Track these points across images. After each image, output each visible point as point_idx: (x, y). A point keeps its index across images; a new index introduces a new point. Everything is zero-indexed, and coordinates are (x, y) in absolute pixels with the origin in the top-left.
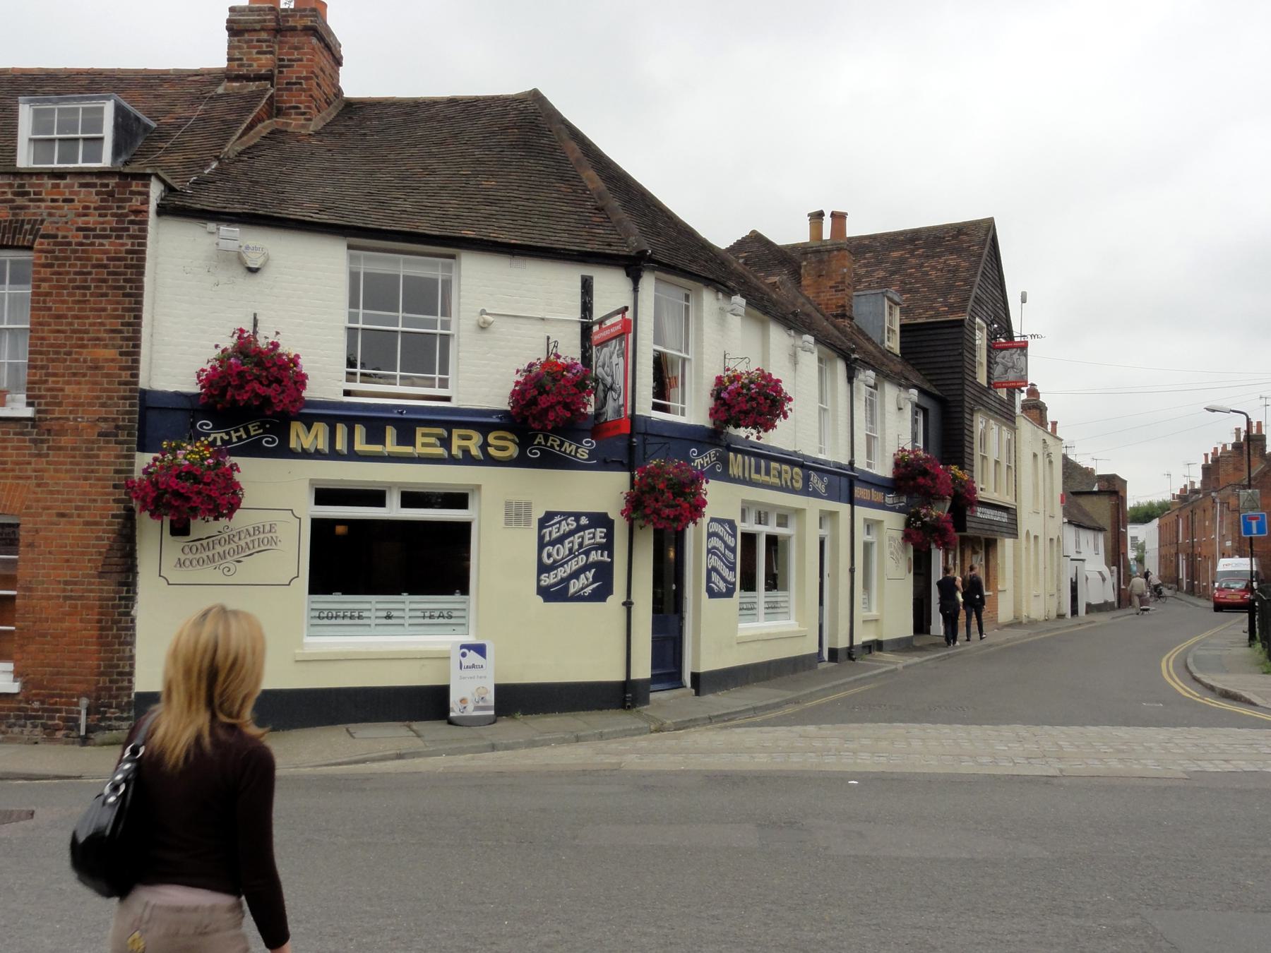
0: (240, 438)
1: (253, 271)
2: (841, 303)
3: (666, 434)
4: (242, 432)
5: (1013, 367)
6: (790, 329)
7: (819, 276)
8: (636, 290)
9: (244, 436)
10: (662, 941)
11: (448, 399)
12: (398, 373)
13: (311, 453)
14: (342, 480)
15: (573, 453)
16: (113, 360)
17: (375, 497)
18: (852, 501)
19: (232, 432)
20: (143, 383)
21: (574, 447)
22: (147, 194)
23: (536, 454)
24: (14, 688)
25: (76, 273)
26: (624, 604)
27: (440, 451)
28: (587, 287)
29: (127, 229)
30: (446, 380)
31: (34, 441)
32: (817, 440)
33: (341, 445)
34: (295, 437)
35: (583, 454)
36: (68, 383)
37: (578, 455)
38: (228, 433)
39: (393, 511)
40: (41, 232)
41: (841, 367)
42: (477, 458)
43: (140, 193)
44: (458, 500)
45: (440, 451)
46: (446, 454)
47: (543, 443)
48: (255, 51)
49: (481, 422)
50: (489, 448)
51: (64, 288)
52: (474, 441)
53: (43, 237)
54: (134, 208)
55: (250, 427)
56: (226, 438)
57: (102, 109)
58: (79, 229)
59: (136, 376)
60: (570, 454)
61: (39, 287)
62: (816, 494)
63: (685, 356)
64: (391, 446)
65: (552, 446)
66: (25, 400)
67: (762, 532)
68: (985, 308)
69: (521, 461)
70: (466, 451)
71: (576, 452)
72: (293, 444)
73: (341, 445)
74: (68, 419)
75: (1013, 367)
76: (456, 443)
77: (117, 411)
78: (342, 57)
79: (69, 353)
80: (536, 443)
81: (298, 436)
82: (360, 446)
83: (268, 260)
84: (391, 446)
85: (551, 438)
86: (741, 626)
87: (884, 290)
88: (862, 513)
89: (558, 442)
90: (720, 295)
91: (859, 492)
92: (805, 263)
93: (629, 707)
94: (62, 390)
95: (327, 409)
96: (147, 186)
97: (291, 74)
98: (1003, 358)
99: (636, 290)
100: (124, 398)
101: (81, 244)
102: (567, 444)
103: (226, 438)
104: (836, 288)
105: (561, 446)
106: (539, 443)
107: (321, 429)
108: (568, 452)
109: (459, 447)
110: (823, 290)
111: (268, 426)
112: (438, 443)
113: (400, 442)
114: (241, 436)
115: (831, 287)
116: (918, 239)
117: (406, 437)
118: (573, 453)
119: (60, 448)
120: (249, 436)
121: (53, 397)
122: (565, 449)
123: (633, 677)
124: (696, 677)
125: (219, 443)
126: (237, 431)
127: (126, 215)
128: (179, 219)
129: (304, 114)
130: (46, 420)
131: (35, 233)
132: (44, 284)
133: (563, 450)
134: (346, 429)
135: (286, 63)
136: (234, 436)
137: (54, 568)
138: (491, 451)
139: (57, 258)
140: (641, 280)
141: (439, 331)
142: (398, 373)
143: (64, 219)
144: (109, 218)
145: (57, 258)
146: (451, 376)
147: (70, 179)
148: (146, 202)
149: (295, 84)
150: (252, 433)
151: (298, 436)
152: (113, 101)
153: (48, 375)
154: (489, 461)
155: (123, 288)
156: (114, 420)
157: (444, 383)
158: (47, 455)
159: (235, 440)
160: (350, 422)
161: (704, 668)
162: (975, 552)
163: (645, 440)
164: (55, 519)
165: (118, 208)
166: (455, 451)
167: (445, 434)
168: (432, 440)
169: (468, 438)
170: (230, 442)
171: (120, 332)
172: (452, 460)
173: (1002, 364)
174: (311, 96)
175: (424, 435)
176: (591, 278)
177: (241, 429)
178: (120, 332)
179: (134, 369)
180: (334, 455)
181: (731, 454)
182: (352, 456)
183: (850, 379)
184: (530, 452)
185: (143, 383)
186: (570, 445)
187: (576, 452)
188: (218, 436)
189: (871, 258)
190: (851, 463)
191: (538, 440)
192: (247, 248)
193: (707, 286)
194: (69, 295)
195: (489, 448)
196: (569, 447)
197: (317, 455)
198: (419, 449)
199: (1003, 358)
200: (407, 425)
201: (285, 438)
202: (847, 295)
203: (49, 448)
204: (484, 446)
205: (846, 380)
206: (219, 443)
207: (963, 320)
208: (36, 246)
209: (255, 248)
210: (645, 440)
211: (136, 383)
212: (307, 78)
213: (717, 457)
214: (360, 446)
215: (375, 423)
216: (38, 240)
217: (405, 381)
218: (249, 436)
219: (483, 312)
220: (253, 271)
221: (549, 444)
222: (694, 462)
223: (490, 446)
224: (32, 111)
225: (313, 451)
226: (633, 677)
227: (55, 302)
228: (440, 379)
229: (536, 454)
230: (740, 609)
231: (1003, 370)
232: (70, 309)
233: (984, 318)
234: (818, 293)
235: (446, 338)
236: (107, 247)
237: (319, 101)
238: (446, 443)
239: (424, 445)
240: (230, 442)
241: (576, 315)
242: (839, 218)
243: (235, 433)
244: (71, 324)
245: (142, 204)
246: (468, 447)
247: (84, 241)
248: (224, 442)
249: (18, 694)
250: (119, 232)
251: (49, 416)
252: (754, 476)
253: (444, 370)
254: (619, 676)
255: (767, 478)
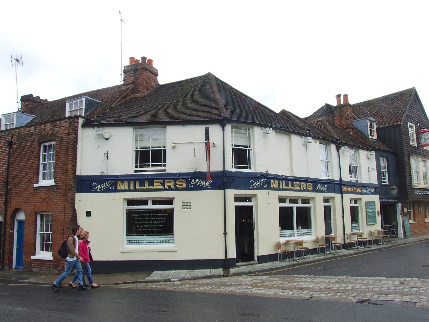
0: (104, 187)
1: (107, 139)
2: (348, 124)
3: (238, 176)
4: (104, 186)
5: (428, 139)
6: (302, 136)
7: (340, 116)
8: (223, 130)
9: (105, 187)
10: (388, 315)
11: (165, 171)
12: (150, 164)
13: (123, 190)
14: (132, 198)
15: (204, 185)
16: (71, 168)
17: (145, 202)
18: (341, 192)
19: (102, 186)
20: (78, 173)
21: (204, 183)
22: (78, 122)
23: (192, 186)
24: (51, 259)
25: (64, 146)
26: (224, 233)
27: (161, 187)
28: (207, 132)
29: (74, 132)
30: (165, 165)
31: (55, 192)
32: (236, 144)
33: (132, 187)
34: (119, 186)
35: (208, 185)
36: (62, 175)
37: (206, 185)
38: (101, 186)
39: (150, 206)
40: (57, 136)
41: (333, 147)
42: (173, 189)
43: (77, 122)
44: (170, 201)
45: (161, 187)
46: (163, 188)
47: (194, 182)
48: (129, 77)
49: (176, 177)
50: (177, 185)
51: (61, 150)
52: (172, 183)
53: (58, 137)
54: (76, 126)
55: (106, 184)
56: (100, 187)
57: (83, 100)
58: (65, 134)
59: (76, 172)
60: (203, 185)
61: (56, 150)
62: (321, 191)
63: (249, 149)
64: (146, 187)
65: (197, 183)
66: (54, 181)
67: (294, 206)
68: (413, 119)
69: (188, 189)
70: (169, 186)
71: (205, 184)
72: (118, 188)
73: (132, 187)
74: (62, 185)
75: (428, 139)
76: (166, 184)
77: (72, 182)
78: (158, 74)
79: (62, 167)
80: (192, 182)
81: (120, 185)
82: (137, 187)
83: (111, 135)
84: (146, 187)
85: (197, 180)
86: (280, 239)
87: (367, 117)
88: (347, 197)
89: (199, 182)
90: (263, 128)
91: (344, 189)
92: (335, 112)
93: (226, 268)
94: (61, 177)
95: (125, 177)
96: (78, 120)
97: (139, 81)
98: (424, 136)
99: (223, 130)
100: (73, 178)
101: (65, 138)
102: (202, 182)
103: (100, 187)
104: (346, 119)
105: (200, 183)
106: (193, 182)
107: (126, 183)
108: (202, 184)
109: (167, 185)
110: (342, 120)
111: (111, 183)
112: (161, 185)
113: (292, 186)
114: (104, 187)
115: (344, 119)
116: (388, 98)
117: (151, 184)
118: (204, 185)
119: (61, 193)
120: (106, 187)
121: (59, 179)
122: (202, 184)
123: (228, 258)
124: (258, 257)
125: (98, 189)
126: (103, 185)
127: (74, 128)
128: (199, 125)
129: (142, 91)
130: (58, 186)
131: (56, 136)
132: (58, 150)
133: (201, 184)
134: (133, 182)
135: (138, 78)
136: (102, 187)
137: (59, 226)
138: (177, 186)
139: (60, 142)
140: (225, 127)
141: (248, 148)
142: (150, 164)
143: (62, 132)
144: (70, 130)
145: (60, 142)
146: (167, 163)
147: (63, 121)
148: (78, 124)
149: (140, 84)
150: (107, 186)
151: (120, 185)
152: (85, 98)
153: (58, 174)
154: (177, 189)
155: (73, 148)
156: (71, 184)
157: (164, 166)
158: (58, 195)
159: (102, 188)
160: (134, 181)
161: (260, 254)
162: (419, 207)
163: (229, 179)
164: (60, 213)
165: (72, 127)
166: (166, 187)
167: (163, 182)
168: (159, 184)
169: (170, 182)
170: (101, 189)
171: (72, 160)
172: (165, 190)
173: (424, 138)
174: (144, 86)
175: (156, 182)
176: (209, 128)
177: (104, 185)
178: (72, 160)
179: (75, 170)
180: (130, 190)
181: (272, 181)
182: (135, 190)
183: (338, 150)
184: (190, 186)
185: (78, 173)
186: (203, 182)
187: (205, 184)
188: (98, 187)
189: (372, 107)
190: (341, 179)
191: (192, 181)
192: (105, 133)
193: (256, 126)
194: (63, 152)
195: (177, 185)
196: (203, 183)
197: (125, 191)
198: (155, 187)
199: (424, 136)
200: (151, 180)
201: (116, 187)
202: (350, 121)
203: (58, 193)
204: (175, 185)
205: (336, 151)
206: (98, 189)
207: (400, 124)
208: (56, 140)
209: (107, 133)
210: (229, 179)
211: (76, 174)
212: (142, 82)
213: (264, 182)
214: (137, 187)
215: (141, 180)
216: (57, 138)
217: (153, 166)
218: (106, 187)
219: (173, 143)
220: (107, 139)
221: (196, 183)
222: (253, 185)
223: (177, 184)
224: (69, 104)
225: (124, 189)
226: (228, 258)
227: (59, 154)
228: (138, 165)
229: (192, 186)
230: (297, 231)
231: (424, 140)
232: (62, 155)
233: (413, 122)
234: (340, 121)
235: (249, 150)
236: (70, 138)
237: (147, 87)
238: (163, 185)
239: (156, 186)
240: (101, 189)
241: (204, 140)
242: (346, 97)
243: (103, 186)
244: (63, 159)
245: (77, 125)
246: (170, 185)
247: (65, 137)
248: (100, 189)
249: (52, 260)
250: (72, 133)
251: (58, 185)
252: (285, 187)
253: (164, 161)
254: (224, 258)
255: (293, 188)
